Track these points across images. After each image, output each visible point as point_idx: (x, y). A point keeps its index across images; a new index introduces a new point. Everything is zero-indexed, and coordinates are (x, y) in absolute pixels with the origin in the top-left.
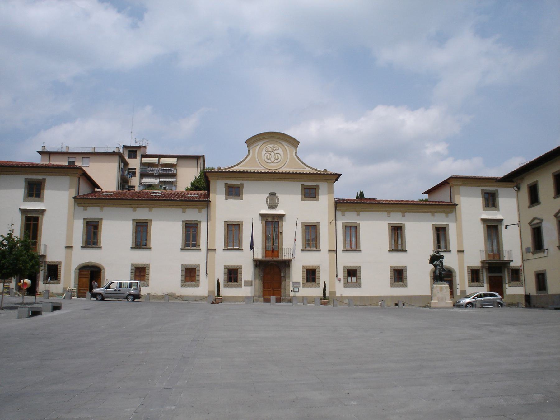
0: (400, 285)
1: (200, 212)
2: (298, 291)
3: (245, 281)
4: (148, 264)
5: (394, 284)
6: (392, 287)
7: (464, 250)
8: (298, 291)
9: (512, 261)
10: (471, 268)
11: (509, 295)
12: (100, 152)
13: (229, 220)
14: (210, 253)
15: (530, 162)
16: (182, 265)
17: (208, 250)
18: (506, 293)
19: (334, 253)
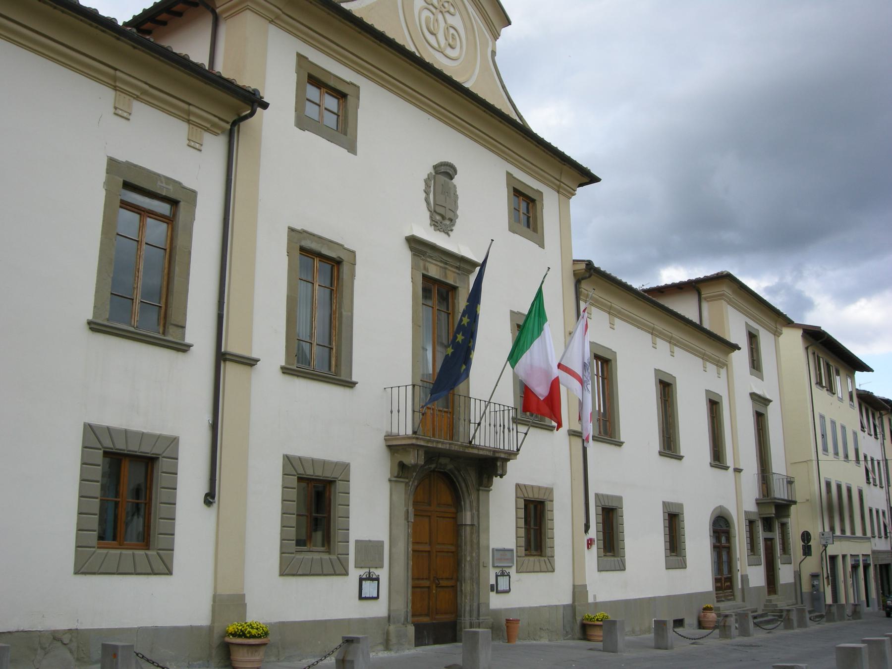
0: (678, 559)
1: (195, 145)
2: (375, 595)
3: (357, 541)
4: (175, 438)
5: (299, 556)
6: (601, 571)
7: (254, 355)
8: (375, 595)
9: (795, 502)
10: (108, 443)
11: (782, 584)
12: (490, 102)
13: (306, 229)
14: (231, 371)
15: (536, 134)
16: (90, 425)
17: (221, 357)
18: (779, 582)
19: (232, 346)
